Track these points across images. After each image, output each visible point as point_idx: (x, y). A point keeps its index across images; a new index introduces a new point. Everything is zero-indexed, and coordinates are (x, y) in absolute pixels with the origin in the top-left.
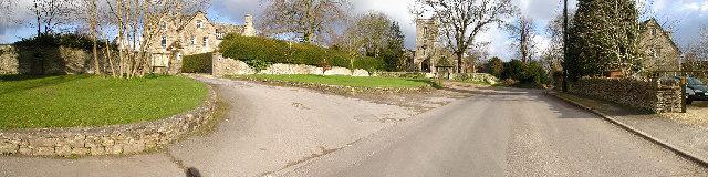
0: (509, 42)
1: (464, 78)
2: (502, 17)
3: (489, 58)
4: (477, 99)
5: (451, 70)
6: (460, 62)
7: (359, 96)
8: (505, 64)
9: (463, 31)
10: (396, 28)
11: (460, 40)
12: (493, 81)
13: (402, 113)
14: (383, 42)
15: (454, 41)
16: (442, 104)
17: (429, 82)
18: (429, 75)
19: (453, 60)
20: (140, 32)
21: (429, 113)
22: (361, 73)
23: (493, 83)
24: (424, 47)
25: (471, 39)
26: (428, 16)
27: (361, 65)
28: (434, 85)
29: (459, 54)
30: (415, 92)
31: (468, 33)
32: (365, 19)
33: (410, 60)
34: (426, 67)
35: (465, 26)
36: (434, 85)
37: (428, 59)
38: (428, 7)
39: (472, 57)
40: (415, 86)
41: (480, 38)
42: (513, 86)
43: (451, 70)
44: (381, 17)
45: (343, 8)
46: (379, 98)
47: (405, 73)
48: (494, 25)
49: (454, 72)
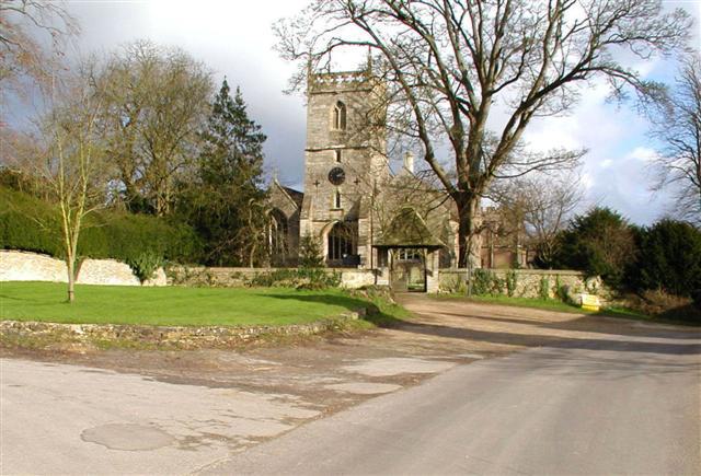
0: (646, 154)
1: (482, 285)
2: (620, 56)
3: (581, 210)
4: (536, 365)
5: (433, 261)
6: (465, 230)
7: (100, 357)
8: (636, 234)
9: (478, 116)
10: (233, 112)
11: (468, 145)
12: (592, 297)
13: (255, 414)
14: (185, 163)
15: (445, 153)
16: (406, 381)
17: (348, 301)
18: (354, 279)
19: (441, 219)
20: (180, 225)
21: (357, 416)
22: (108, 273)
23: (592, 302)
24: (336, 176)
25: (507, 142)
26: (349, 60)
27: (105, 241)
28: (373, 314)
29: (464, 197)
30: (305, 341)
31: (496, 121)
32: (118, 71)
33: (289, 225)
34: (344, 249)
35: (487, 94)
36: (373, 314)
37: (353, 218)
38: (354, 32)
39: (516, 210)
40: (313, 317)
41: (543, 136)
42: (672, 316)
43: (433, 261)
44: (179, 68)
45: (42, 38)
46: (182, 367)
47: (266, 270)
48: (596, 88)
49: (445, 263)
